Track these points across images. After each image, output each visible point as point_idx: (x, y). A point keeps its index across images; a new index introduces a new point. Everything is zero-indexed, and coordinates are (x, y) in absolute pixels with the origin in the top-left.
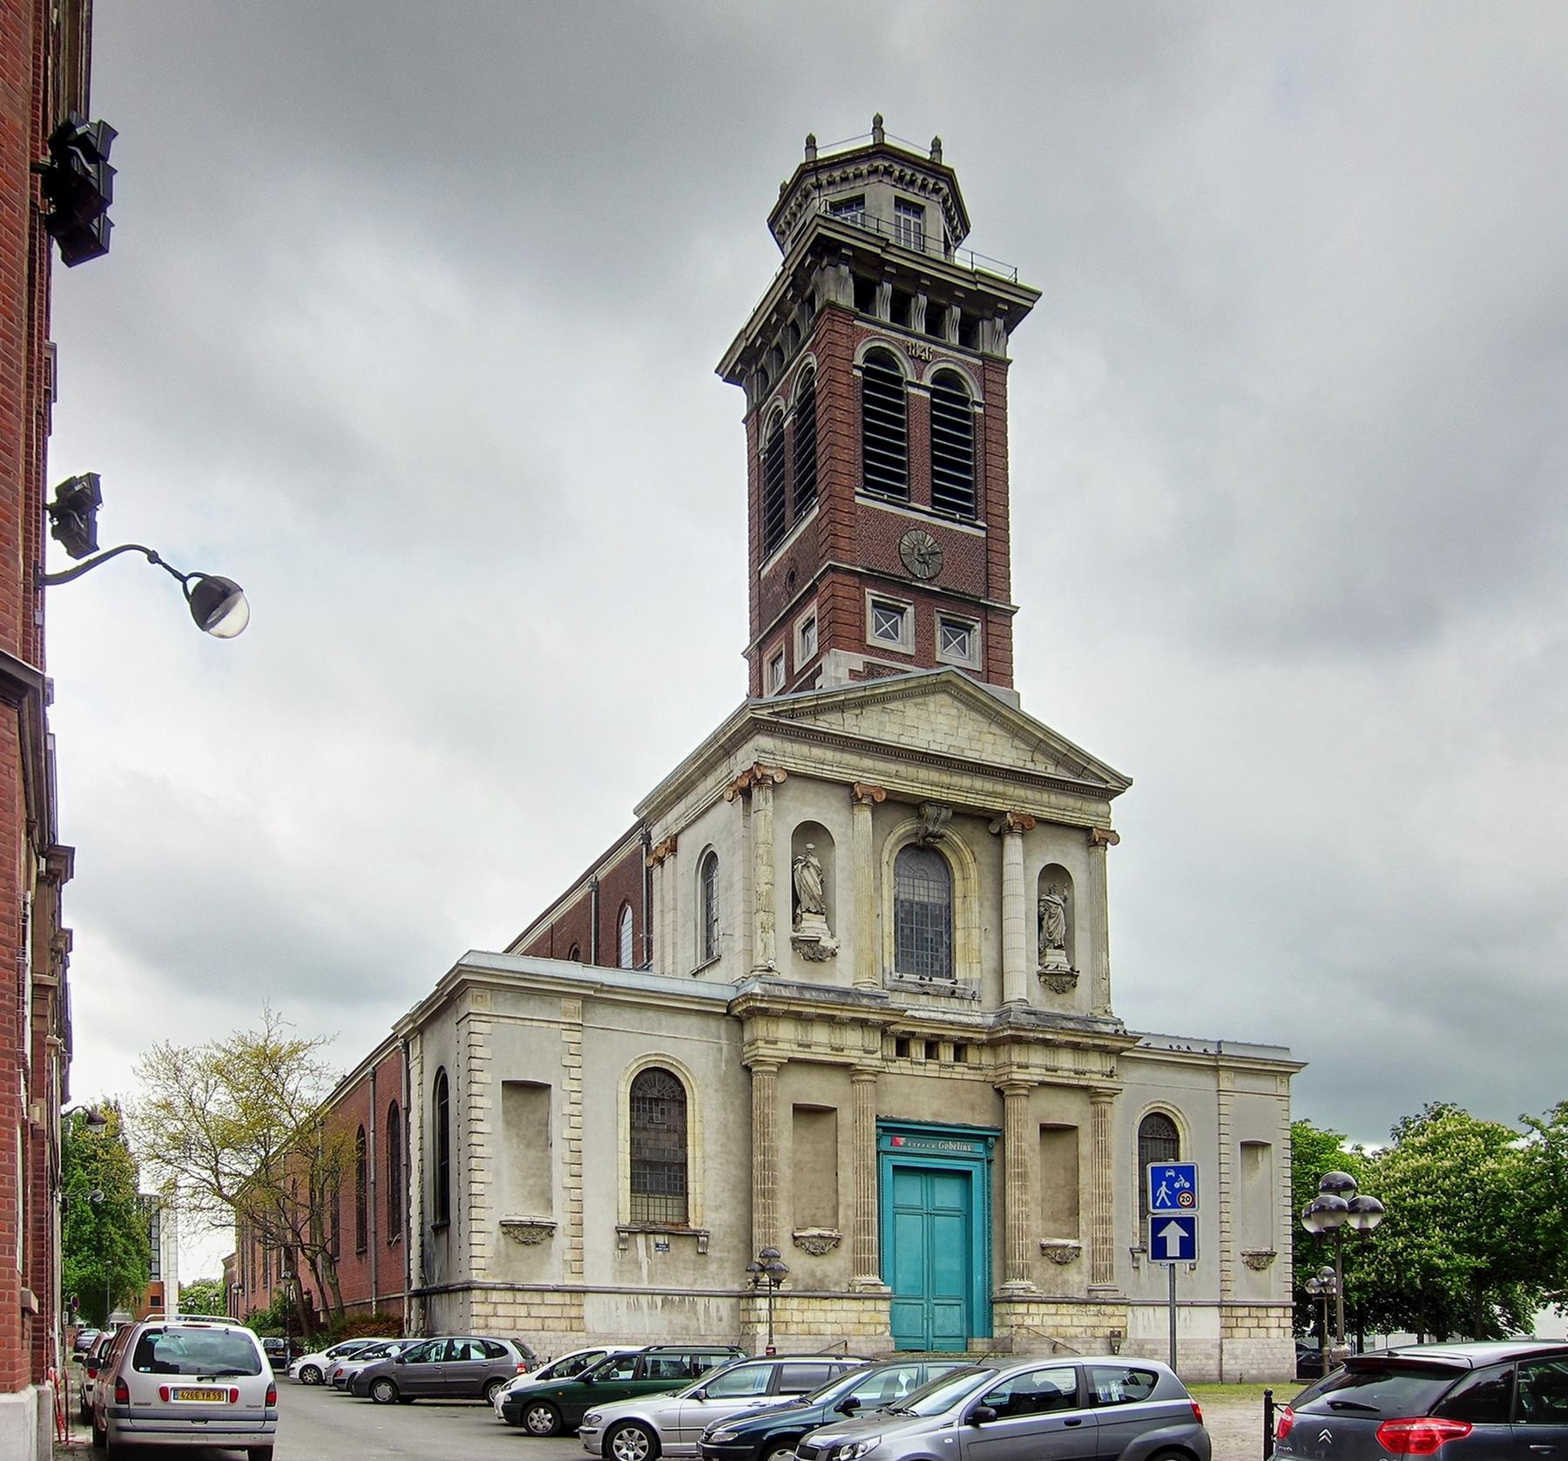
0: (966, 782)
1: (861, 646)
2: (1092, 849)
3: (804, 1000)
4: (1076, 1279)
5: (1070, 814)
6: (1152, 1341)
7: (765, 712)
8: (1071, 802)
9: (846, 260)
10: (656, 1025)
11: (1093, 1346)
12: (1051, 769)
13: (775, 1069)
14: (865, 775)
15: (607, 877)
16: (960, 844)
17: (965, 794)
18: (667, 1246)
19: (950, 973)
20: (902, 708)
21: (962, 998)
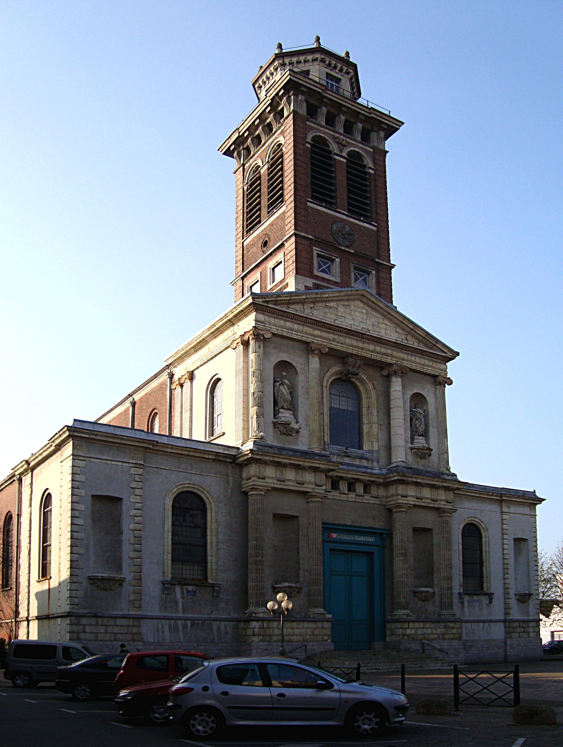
1: (313, 276)
2: (438, 387)
5: (426, 368)
7: (260, 300)
9: (303, 93)
10: (189, 467)
11: (444, 644)
12: (416, 344)
13: (263, 493)
14: (316, 338)
16: (366, 379)
17: (371, 353)
18: (195, 592)
19: (360, 447)
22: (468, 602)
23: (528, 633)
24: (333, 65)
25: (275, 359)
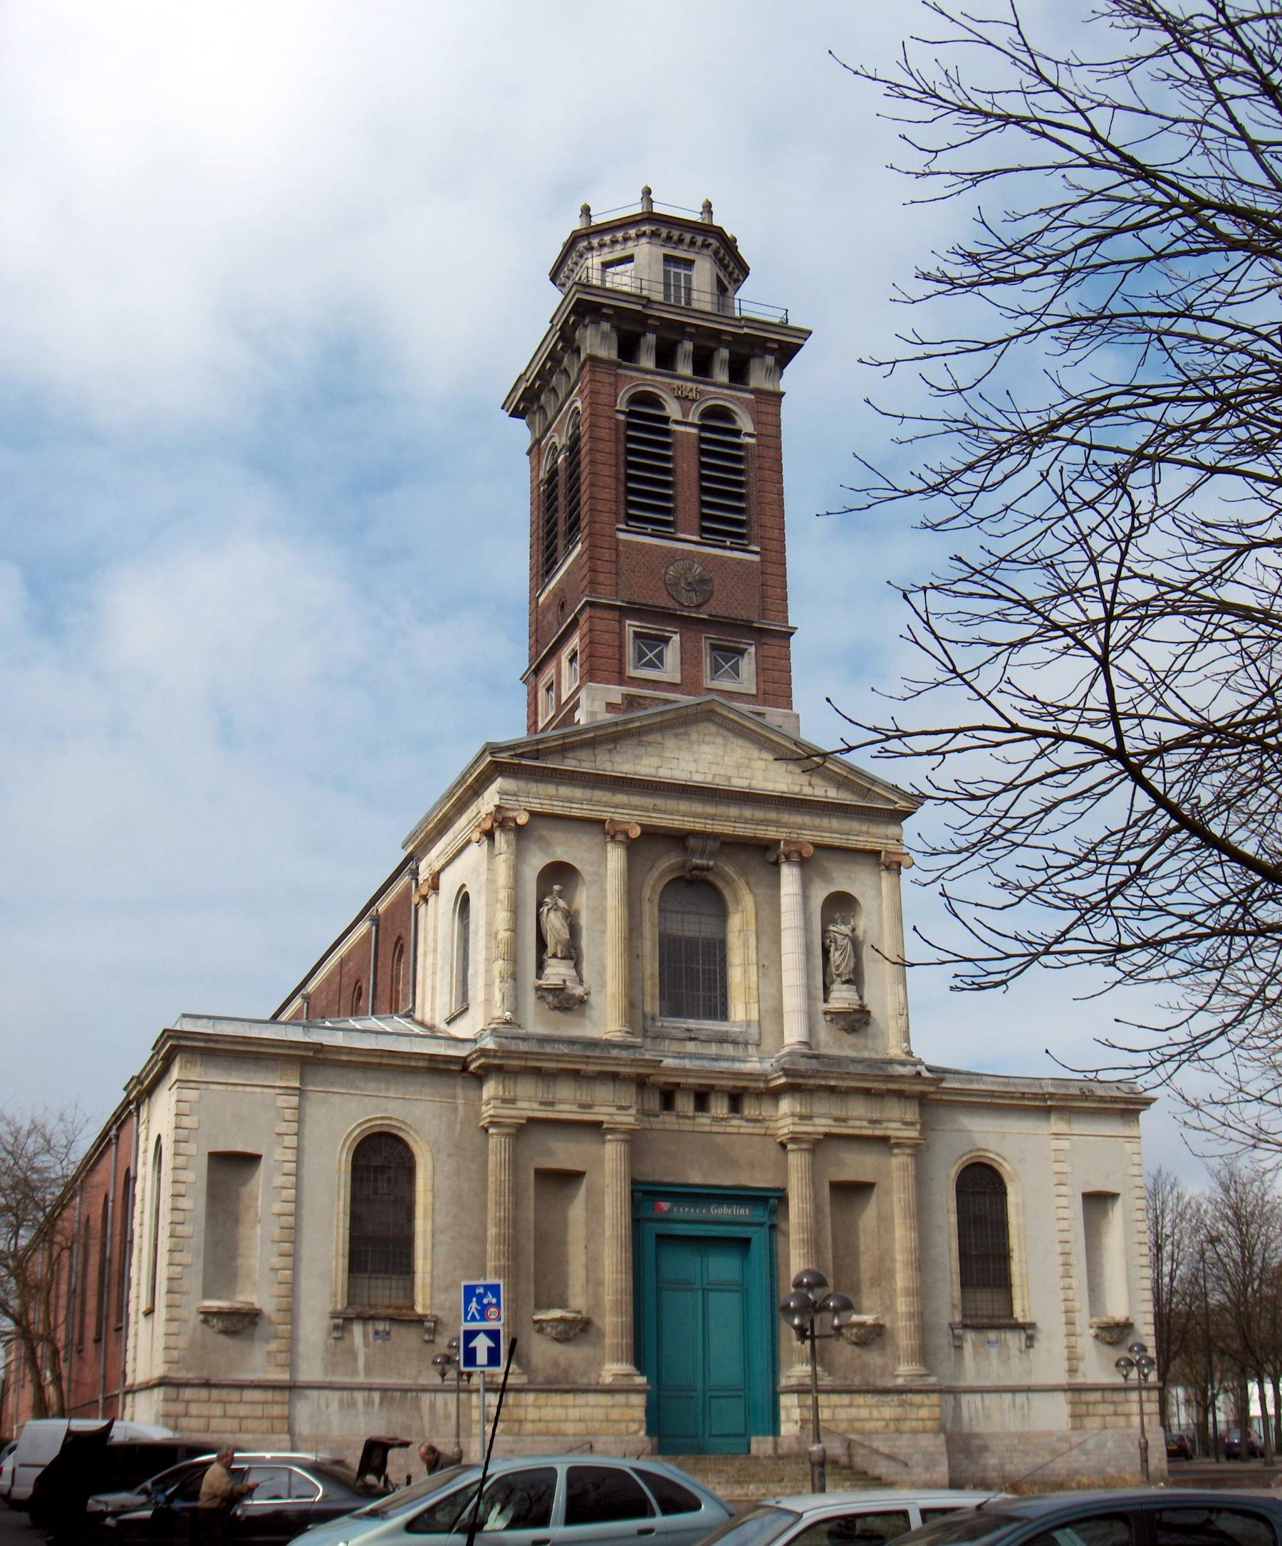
0: (734, 811)
1: (622, 679)
7: (505, 755)
8: (855, 825)
9: (607, 318)
11: (898, 1443)
15: (386, 911)
18: (388, 1333)
22: (974, 1346)
23: (1127, 1415)
24: (675, 238)
25: (537, 862)
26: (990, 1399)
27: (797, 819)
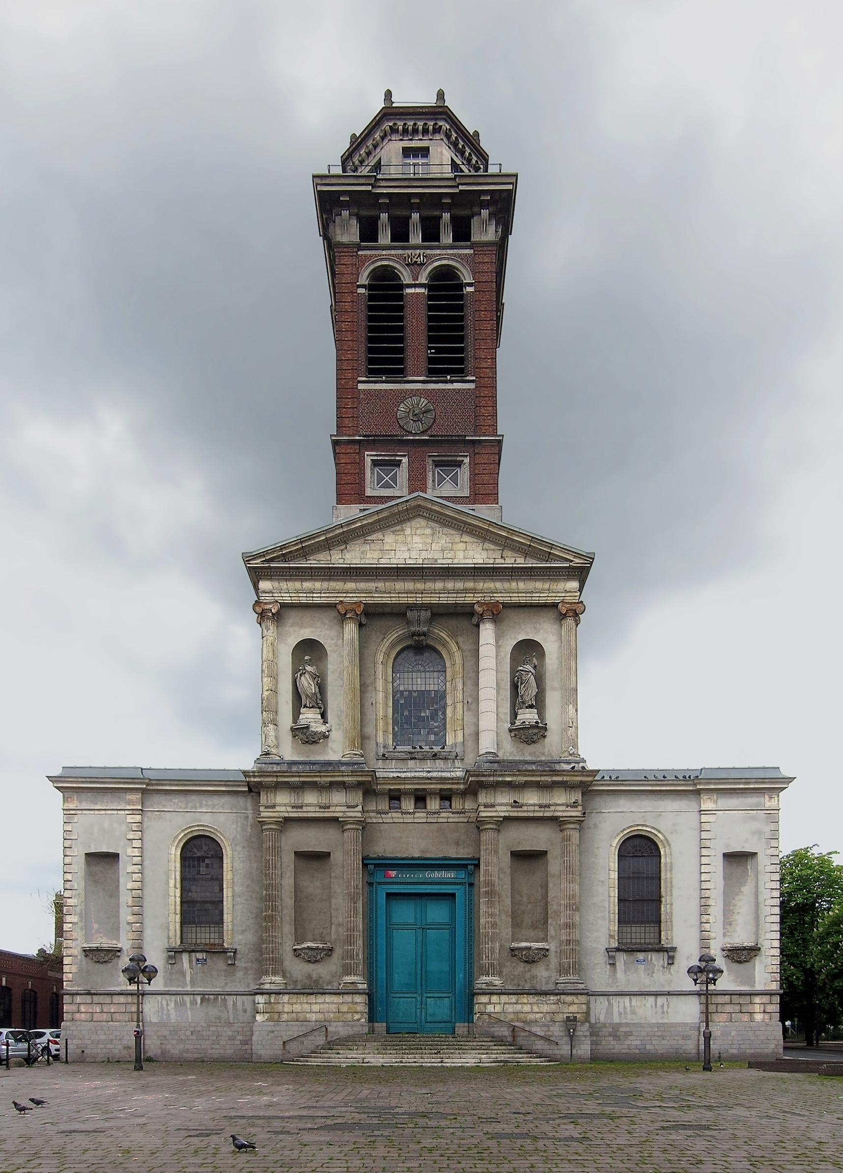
3: (291, 772)
4: (543, 974)
6: (627, 1024)
10: (198, 805)
11: (551, 1029)
18: (205, 960)
20: (381, 537)
21: (445, 759)
22: (625, 963)
26: (635, 1001)
27: (490, 585)
